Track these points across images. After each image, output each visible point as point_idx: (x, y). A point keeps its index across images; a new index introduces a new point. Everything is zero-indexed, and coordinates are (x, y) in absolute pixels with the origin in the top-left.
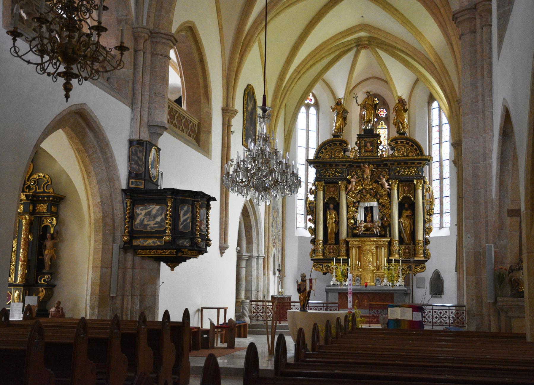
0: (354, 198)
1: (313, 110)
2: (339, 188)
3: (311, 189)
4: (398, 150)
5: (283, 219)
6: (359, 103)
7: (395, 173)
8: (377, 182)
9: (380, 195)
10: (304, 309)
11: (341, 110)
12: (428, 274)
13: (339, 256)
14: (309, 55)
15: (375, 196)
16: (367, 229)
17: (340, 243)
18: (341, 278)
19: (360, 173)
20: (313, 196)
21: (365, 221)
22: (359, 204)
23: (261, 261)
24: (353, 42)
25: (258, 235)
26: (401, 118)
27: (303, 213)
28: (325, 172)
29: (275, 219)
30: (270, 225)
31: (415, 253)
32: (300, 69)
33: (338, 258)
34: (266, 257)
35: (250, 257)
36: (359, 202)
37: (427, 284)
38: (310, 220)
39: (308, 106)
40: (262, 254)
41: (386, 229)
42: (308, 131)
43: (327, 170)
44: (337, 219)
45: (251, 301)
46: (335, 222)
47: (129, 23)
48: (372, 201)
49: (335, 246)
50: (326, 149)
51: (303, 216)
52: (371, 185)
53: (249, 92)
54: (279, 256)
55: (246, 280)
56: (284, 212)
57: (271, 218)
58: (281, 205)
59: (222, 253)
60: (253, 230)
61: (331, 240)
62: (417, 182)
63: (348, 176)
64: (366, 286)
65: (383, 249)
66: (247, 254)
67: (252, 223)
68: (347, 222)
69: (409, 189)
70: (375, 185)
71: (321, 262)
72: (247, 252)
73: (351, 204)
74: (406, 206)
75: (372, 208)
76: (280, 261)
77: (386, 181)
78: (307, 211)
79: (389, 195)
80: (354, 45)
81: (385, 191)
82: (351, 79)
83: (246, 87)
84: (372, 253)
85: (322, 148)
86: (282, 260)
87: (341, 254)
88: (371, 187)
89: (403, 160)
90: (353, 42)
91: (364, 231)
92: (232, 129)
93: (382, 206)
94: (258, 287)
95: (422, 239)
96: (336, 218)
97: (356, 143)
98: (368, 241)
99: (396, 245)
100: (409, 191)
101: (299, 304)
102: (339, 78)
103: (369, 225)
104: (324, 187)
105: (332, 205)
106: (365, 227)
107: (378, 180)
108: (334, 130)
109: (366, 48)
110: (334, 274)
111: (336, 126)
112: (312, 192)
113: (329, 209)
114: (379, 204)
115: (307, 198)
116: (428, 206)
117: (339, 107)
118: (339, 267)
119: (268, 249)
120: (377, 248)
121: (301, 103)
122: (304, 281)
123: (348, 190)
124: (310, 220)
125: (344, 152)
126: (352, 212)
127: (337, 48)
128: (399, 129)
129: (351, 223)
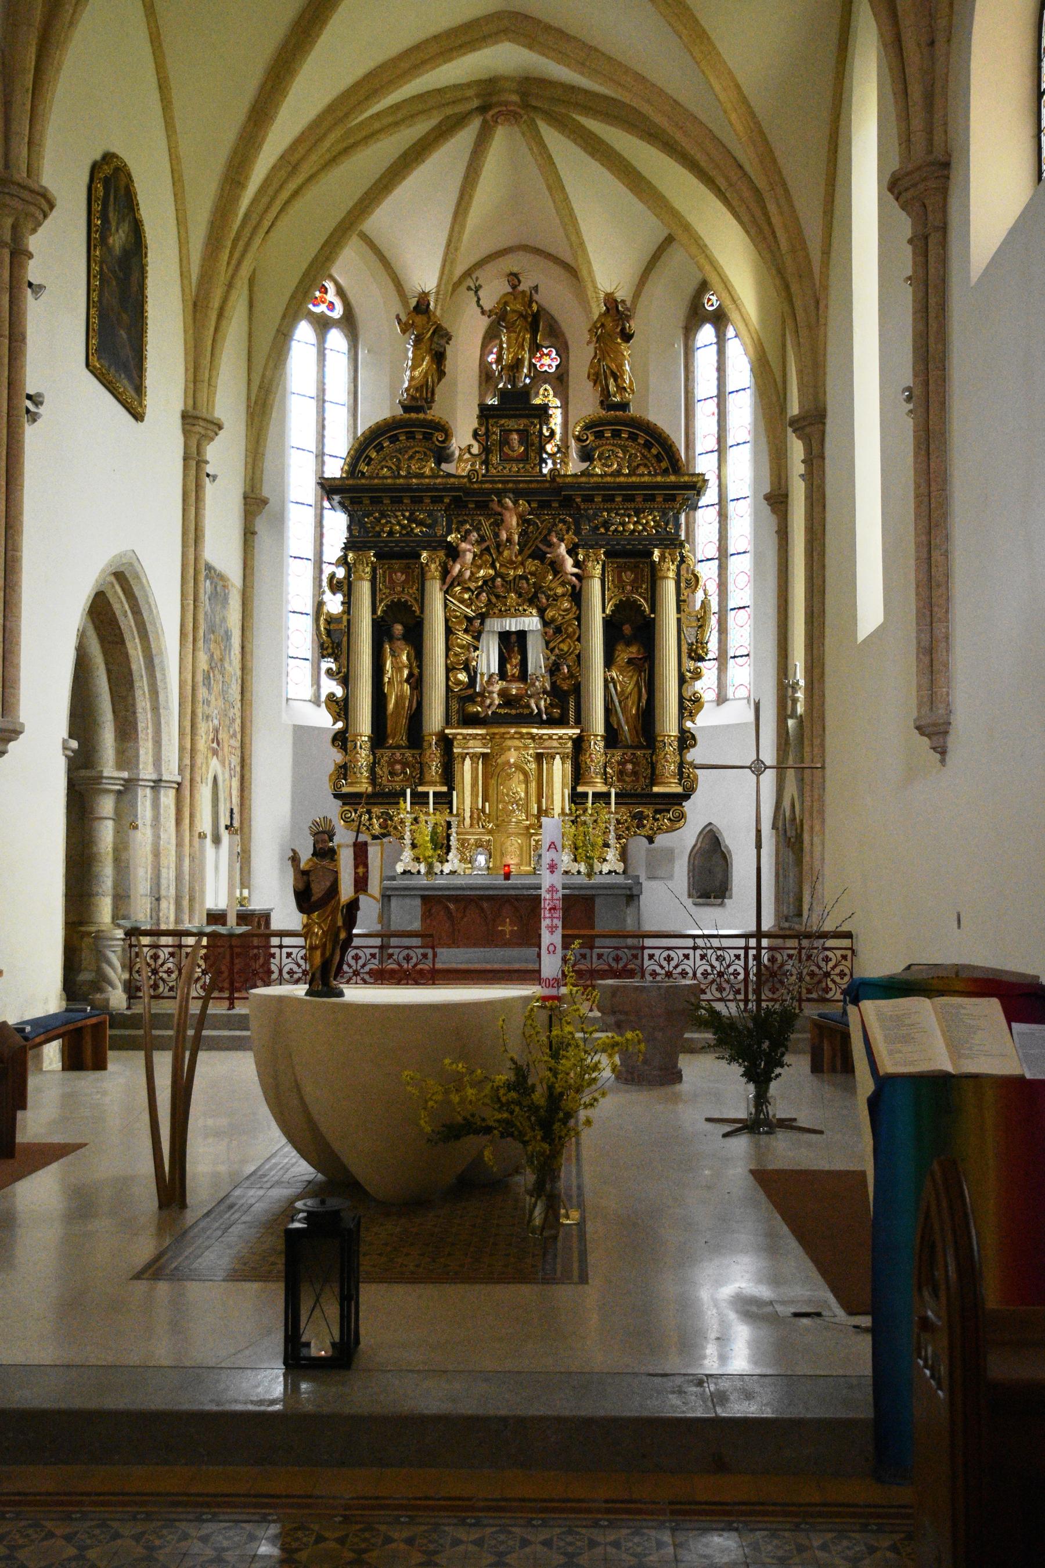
0: (469, 604)
1: (336, 339)
2: (423, 570)
3: (332, 576)
4: (605, 460)
5: (243, 669)
6: (487, 308)
8: (539, 555)
9: (548, 597)
10: (326, 982)
11: (426, 328)
12: (686, 838)
13: (421, 785)
14: (330, 109)
16: (508, 700)
17: (425, 744)
18: (430, 853)
19: (486, 525)
20: (339, 597)
21: (502, 674)
22: (482, 623)
23: (168, 798)
24: (470, 93)
25: (156, 709)
26: (613, 360)
27: (309, 656)
28: (378, 520)
29: (216, 665)
30: (200, 678)
31: (653, 773)
32: (297, 156)
33: (420, 789)
34: (187, 783)
35: (130, 786)
36: (483, 617)
37: (681, 870)
38: (329, 672)
39: (322, 325)
40: (171, 771)
41: (565, 700)
42: (324, 401)
43: (383, 515)
44: (416, 671)
45: (133, 932)
46: (407, 681)
49: (408, 753)
50: (379, 448)
51: (308, 664)
52: (522, 564)
53: (111, 190)
54: (230, 786)
55: (117, 860)
56: (248, 646)
57: (203, 658)
58: (239, 625)
60: (138, 693)
61: (398, 736)
62: (662, 557)
63: (449, 533)
64: (507, 876)
66: (116, 774)
67: (134, 667)
68: (448, 679)
69: (634, 581)
70: (532, 565)
71: (370, 801)
72: (120, 765)
73: (460, 623)
74: (627, 629)
75: (522, 635)
76: (236, 800)
77: (569, 552)
78: (322, 646)
79: (577, 597)
80: (476, 103)
81: (563, 584)
82: (461, 232)
83: (98, 156)
84: (526, 774)
85: (368, 446)
86: (242, 797)
87: (427, 778)
88: (520, 572)
89: (620, 487)
90: (470, 93)
91: (499, 706)
92: (34, 272)
93: (553, 629)
94: (158, 885)
95: (674, 732)
96: (411, 668)
97: (475, 435)
98: (512, 738)
99: (597, 747)
100: (635, 586)
101: (300, 941)
102: (419, 236)
104: (374, 570)
105: (400, 625)
106: (503, 693)
107: (544, 548)
108: (407, 390)
109: (512, 116)
110: (408, 841)
111: (412, 379)
112: (335, 586)
113: (391, 639)
114: (545, 624)
115: (320, 605)
116: (693, 631)
117: (420, 320)
118: (422, 818)
119: (192, 758)
120: (539, 757)
121: (295, 309)
122: (324, 852)
123: (449, 580)
124: (329, 672)
125: (438, 463)
126: (462, 647)
127: (420, 107)
128: (606, 393)
129: (459, 682)
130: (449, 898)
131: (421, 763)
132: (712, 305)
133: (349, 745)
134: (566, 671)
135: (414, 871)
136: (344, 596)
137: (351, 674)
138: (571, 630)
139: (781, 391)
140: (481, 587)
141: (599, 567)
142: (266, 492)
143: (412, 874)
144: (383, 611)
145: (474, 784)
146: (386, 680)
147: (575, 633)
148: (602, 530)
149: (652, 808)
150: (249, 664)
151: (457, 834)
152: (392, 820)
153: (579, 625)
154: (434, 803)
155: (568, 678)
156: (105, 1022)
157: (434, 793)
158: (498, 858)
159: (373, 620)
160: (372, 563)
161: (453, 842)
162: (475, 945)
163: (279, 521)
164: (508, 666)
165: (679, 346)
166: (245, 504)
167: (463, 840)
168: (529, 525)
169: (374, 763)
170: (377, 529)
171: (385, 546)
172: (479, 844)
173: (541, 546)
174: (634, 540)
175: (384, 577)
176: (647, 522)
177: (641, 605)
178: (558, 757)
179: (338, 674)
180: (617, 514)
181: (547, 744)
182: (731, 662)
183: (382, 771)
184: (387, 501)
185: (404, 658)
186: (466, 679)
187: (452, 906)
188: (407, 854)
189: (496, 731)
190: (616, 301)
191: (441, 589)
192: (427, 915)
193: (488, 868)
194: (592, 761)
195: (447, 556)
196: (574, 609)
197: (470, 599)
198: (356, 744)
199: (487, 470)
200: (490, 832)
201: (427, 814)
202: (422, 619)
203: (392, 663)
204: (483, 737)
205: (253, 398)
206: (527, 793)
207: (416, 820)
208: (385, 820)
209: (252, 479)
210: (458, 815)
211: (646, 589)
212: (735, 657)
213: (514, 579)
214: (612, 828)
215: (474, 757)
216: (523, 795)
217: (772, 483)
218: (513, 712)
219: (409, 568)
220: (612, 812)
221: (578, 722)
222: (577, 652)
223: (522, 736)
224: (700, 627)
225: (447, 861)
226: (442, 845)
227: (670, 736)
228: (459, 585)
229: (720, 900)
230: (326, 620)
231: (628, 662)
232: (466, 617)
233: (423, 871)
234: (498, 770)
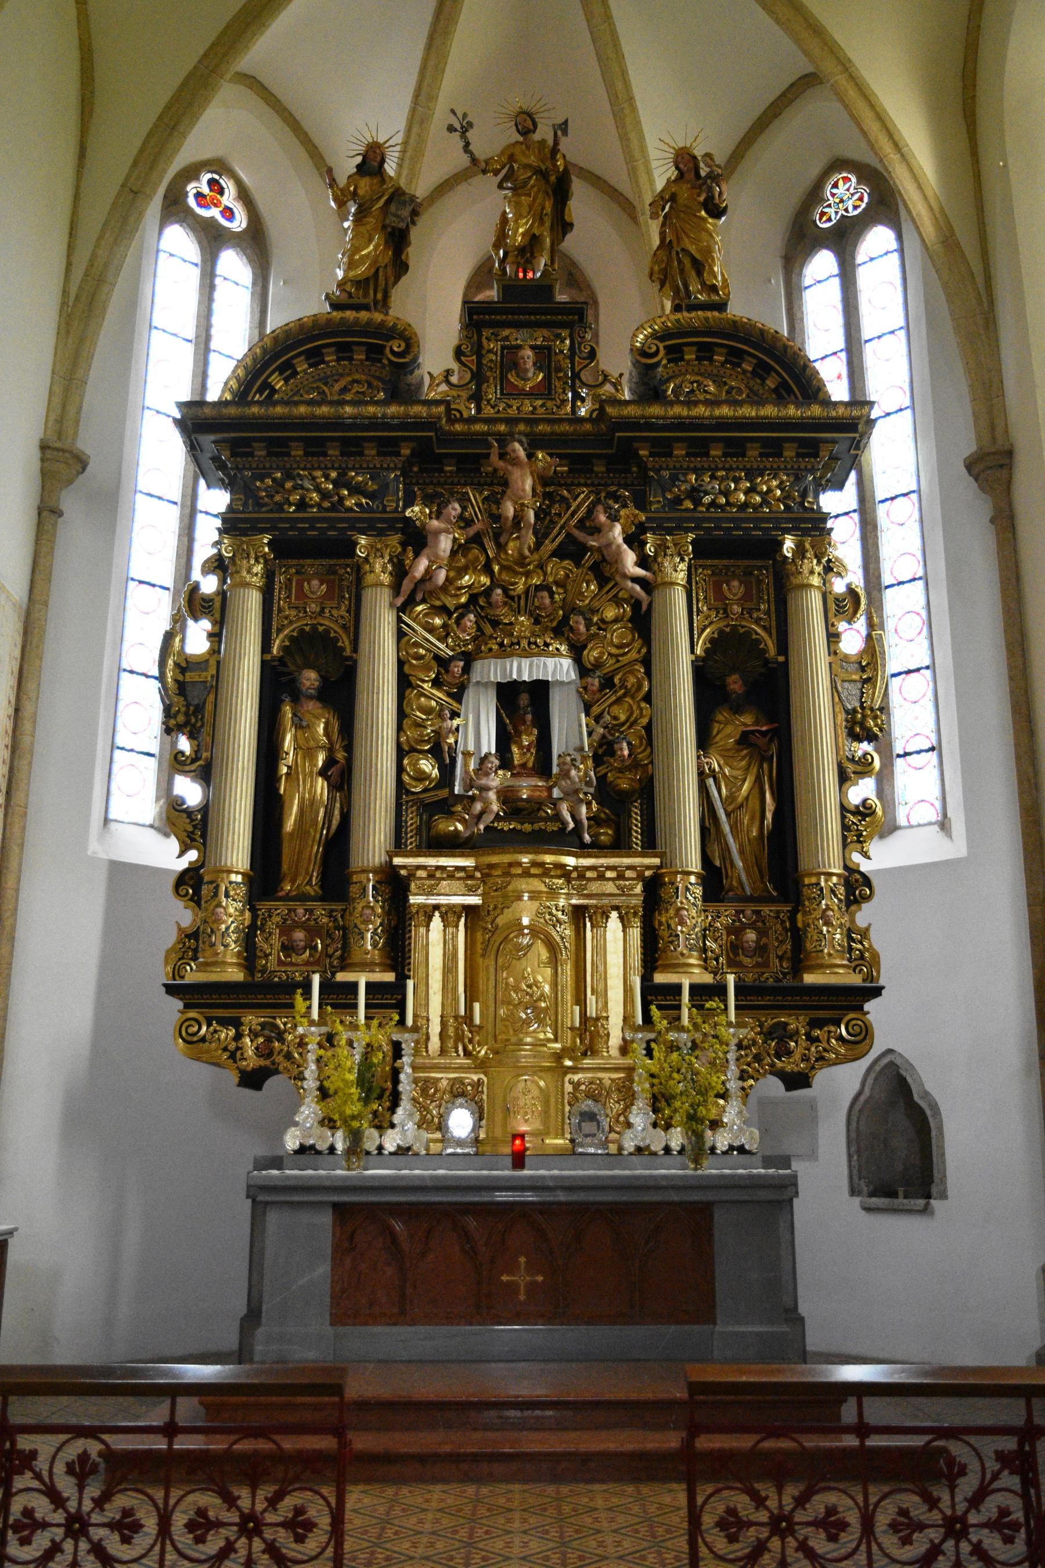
1: (233, 265)
7: (678, 501)
8: (571, 551)
13: (343, 969)
15: (562, 628)
17: (354, 889)
18: (354, 1108)
20: (206, 624)
22: (467, 670)
28: (279, 484)
33: (341, 977)
36: (468, 659)
39: (212, 239)
41: (627, 807)
42: (207, 350)
44: (340, 755)
46: (323, 773)
48: (544, 651)
49: (320, 911)
56: (28, 709)
59: (869, 858)
61: (303, 872)
62: (800, 551)
63: (409, 503)
64: (519, 1160)
65: (614, 922)
68: (400, 769)
70: (557, 569)
75: (540, 689)
77: (629, 540)
79: (643, 622)
81: (617, 601)
84: (552, 948)
87: (356, 957)
88: (536, 581)
93: (598, 684)
96: (330, 751)
97: (458, 353)
98: (526, 874)
99: (689, 895)
103: (527, 788)
104: (269, 576)
105: (312, 672)
106: (507, 796)
110: (311, 1083)
114: (583, 671)
117: (365, 185)
118: (344, 1036)
120: (578, 914)
123: (407, 586)
129: (421, 776)
130: (396, 1209)
131: (344, 928)
132: (829, 220)
133: (205, 890)
134: (626, 752)
135: (323, 1146)
136: (214, 623)
137: (216, 763)
138: (632, 680)
139: (982, 291)
140: (465, 606)
141: (683, 566)
142: (85, 444)
143: (319, 1153)
144: (283, 648)
145: (449, 969)
147: (640, 686)
148: (689, 504)
150: (26, 740)
151: (415, 1068)
152: (281, 1039)
153: (648, 673)
154: (368, 1006)
155: (629, 769)
157: (368, 985)
158: (499, 1117)
159: (264, 664)
160: (264, 556)
161: (405, 1085)
162: (449, 1319)
163: (111, 505)
164: (515, 749)
165: (778, 285)
166: (42, 460)
167: (426, 1080)
168: (553, 502)
169: (253, 927)
170: (278, 498)
171: (291, 529)
172: (458, 1093)
173: (576, 533)
174: (748, 520)
175: (288, 588)
176: (770, 490)
177: (758, 642)
178: (614, 915)
179: (193, 761)
180: (713, 477)
181: (595, 887)
182: (899, 763)
183: (271, 946)
184: (298, 452)
185: (321, 729)
186: (435, 773)
187: (398, 1227)
188: (309, 1112)
189: (495, 859)
190: (695, 158)
191: (392, 605)
192: (345, 1247)
193: (477, 1141)
194: (682, 923)
195: (404, 544)
196: (637, 644)
197: (445, 626)
198: (217, 887)
199: (479, 409)
200: (482, 1065)
201: (354, 1027)
202: (355, 662)
203: (295, 738)
204: (468, 874)
205: (73, 291)
206: (554, 984)
207: (330, 1039)
208: (269, 1040)
209: (60, 421)
210: (415, 1029)
211: (768, 613)
212: (906, 754)
213: (527, 592)
214: (732, 1056)
215: (450, 915)
216: (547, 989)
217: (979, 437)
218: (527, 827)
219: (335, 573)
220: (730, 1022)
221: (650, 844)
222: (644, 721)
223: (545, 872)
224: (868, 680)
225: (393, 1126)
226: (381, 1092)
227: (830, 875)
228: (424, 601)
229: (921, 1202)
230: (177, 665)
231: (738, 742)
232: (437, 658)
233: (340, 1147)
234: (498, 939)
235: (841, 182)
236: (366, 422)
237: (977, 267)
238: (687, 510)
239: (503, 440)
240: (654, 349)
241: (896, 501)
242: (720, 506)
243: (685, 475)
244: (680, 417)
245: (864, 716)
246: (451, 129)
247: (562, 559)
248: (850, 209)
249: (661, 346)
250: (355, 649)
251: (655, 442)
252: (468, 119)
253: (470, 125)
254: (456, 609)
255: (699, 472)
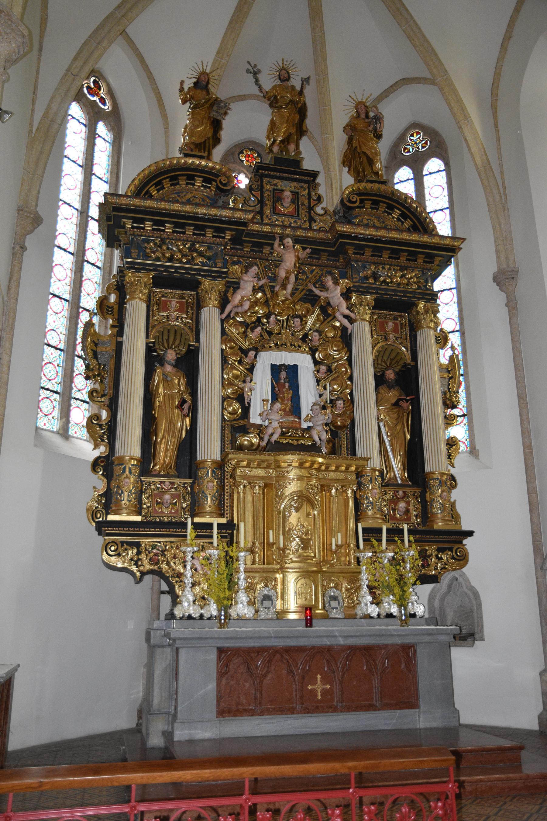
7: (366, 278)
47: (127, 798)
59: (454, 467)
75: (293, 370)
79: (345, 339)
93: (326, 371)
132: (409, 152)
142: (41, 211)
146: (157, 404)
148: (371, 281)
149: (435, 547)
156: (104, 106)
171: (165, 271)
180: (383, 268)
224: (451, 378)
232: (240, 349)
235: (415, 134)
236: (211, 217)
237: (500, 181)
238: (371, 283)
239: (282, 238)
240: (355, 199)
241: (443, 293)
242: (388, 283)
243: (370, 266)
244: (372, 235)
245: (450, 396)
246: (248, 71)
247: (305, 302)
248: (420, 147)
249: (358, 198)
250: (198, 340)
251: (358, 247)
252: (258, 67)
253: (259, 71)
254: (251, 324)
255: (376, 264)
